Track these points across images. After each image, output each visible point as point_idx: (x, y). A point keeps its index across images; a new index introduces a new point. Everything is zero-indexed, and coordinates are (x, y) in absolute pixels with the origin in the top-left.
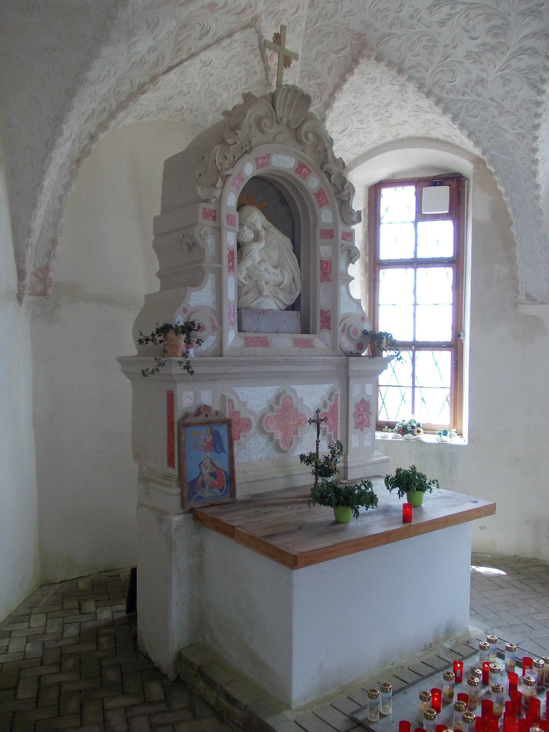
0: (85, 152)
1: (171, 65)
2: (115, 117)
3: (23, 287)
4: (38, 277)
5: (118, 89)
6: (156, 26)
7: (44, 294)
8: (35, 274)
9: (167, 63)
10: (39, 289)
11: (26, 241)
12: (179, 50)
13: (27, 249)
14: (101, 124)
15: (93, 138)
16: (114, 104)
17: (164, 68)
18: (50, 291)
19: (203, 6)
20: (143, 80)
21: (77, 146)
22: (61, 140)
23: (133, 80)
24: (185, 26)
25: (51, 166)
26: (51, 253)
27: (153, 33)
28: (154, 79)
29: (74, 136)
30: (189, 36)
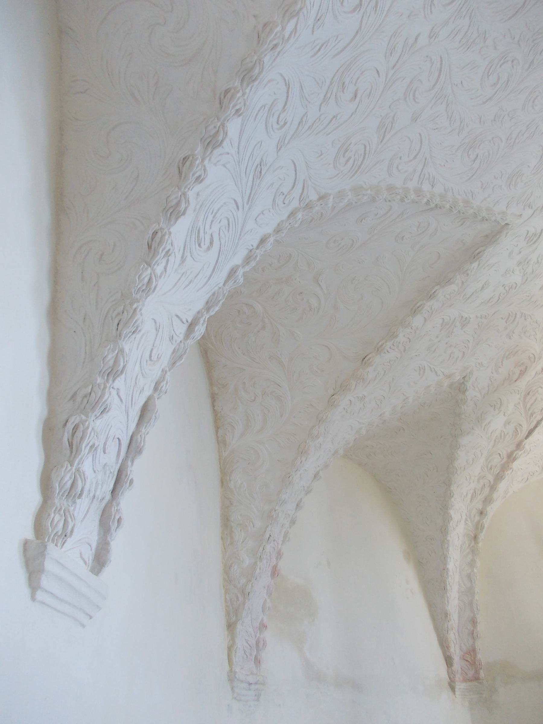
0: (479, 527)
1: (530, 428)
2: (496, 488)
3: (453, 673)
4: (467, 661)
5: (489, 466)
6: (501, 405)
7: (476, 678)
8: (463, 658)
9: (525, 429)
10: (471, 673)
11: (446, 626)
12: (532, 415)
13: (449, 633)
14: (486, 499)
15: (482, 513)
16: (491, 478)
17: (525, 432)
18: (482, 674)
19: (536, 373)
20: (509, 450)
21: (470, 524)
22: (452, 524)
23: (501, 453)
24: (528, 394)
25: (451, 549)
26: (474, 633)
27: (501, 410)
28: (519, 446)
29: (464, 517)
30: (535, 400)
